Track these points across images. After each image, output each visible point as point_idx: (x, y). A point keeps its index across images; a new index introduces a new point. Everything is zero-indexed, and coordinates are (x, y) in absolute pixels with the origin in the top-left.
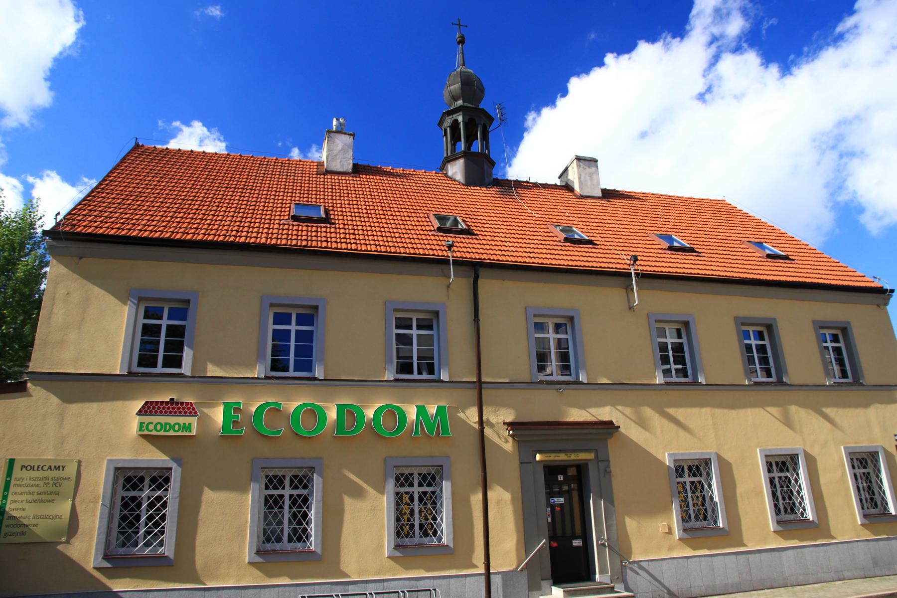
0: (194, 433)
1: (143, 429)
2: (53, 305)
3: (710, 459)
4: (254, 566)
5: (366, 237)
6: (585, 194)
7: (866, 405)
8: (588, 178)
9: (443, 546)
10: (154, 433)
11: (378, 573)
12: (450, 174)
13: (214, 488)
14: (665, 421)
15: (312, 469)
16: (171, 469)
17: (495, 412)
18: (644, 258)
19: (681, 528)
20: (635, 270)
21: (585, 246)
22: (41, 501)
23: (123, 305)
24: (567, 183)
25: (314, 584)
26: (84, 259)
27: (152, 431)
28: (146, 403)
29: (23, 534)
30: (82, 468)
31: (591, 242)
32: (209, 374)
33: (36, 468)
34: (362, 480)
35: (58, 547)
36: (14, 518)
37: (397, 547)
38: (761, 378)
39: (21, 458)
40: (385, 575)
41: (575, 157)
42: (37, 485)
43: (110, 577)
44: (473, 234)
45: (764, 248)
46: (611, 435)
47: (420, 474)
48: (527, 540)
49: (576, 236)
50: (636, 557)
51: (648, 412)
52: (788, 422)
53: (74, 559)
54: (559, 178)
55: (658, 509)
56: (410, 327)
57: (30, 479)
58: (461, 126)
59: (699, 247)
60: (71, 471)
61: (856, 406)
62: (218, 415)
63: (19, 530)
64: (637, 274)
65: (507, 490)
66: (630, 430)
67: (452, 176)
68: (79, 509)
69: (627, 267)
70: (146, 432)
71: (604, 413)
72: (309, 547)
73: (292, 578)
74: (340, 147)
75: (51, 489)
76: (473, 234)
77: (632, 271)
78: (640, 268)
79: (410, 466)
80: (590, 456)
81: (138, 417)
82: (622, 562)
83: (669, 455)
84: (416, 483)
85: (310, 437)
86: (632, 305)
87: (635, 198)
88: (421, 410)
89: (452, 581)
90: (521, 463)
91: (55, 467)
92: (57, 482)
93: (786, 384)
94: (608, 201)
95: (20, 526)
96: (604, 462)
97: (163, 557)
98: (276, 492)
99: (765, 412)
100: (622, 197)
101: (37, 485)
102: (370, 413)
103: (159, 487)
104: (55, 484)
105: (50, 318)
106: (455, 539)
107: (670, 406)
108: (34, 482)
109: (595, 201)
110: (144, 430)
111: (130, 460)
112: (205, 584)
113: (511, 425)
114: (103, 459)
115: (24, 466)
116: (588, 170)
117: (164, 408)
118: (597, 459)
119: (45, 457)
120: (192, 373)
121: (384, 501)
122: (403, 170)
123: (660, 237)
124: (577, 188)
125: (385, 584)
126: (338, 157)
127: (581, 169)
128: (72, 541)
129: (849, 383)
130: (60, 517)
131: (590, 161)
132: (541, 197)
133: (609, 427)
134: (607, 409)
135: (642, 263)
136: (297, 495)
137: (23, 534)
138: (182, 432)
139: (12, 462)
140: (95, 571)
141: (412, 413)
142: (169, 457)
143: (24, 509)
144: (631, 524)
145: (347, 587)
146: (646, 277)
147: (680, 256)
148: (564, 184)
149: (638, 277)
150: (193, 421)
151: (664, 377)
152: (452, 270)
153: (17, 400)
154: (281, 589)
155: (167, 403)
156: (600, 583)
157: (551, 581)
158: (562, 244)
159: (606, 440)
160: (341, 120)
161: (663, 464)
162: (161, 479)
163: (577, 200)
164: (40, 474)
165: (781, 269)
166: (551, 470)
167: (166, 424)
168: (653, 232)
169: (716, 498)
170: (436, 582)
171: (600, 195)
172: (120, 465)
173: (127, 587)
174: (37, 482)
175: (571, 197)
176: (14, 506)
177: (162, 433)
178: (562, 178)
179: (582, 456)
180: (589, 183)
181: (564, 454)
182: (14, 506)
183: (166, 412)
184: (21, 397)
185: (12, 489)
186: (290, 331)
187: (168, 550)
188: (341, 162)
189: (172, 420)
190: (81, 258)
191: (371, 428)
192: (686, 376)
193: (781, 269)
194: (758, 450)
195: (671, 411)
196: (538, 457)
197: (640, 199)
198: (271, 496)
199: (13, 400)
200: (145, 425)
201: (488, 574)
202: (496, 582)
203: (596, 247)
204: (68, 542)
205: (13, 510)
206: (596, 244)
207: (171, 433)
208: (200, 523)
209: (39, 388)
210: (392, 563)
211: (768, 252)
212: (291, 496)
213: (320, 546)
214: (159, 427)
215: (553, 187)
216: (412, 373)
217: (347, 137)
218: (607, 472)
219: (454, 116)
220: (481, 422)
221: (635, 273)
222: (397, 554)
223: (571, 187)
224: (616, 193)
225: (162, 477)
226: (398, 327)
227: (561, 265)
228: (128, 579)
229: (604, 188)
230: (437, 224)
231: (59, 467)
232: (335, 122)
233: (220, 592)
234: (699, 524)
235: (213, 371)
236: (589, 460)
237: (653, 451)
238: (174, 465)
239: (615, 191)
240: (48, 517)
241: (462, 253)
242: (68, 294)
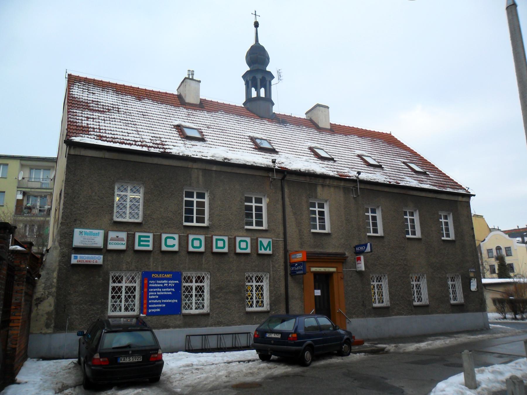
24: (311, 118)
54: (306, 114)
84: (194, 280)
148: (309, 118)
178: (309, 114)
186: (197, 202)
198: (198, 286)
212: (256, 286)
216: (252, 225)
229: (334, 123)
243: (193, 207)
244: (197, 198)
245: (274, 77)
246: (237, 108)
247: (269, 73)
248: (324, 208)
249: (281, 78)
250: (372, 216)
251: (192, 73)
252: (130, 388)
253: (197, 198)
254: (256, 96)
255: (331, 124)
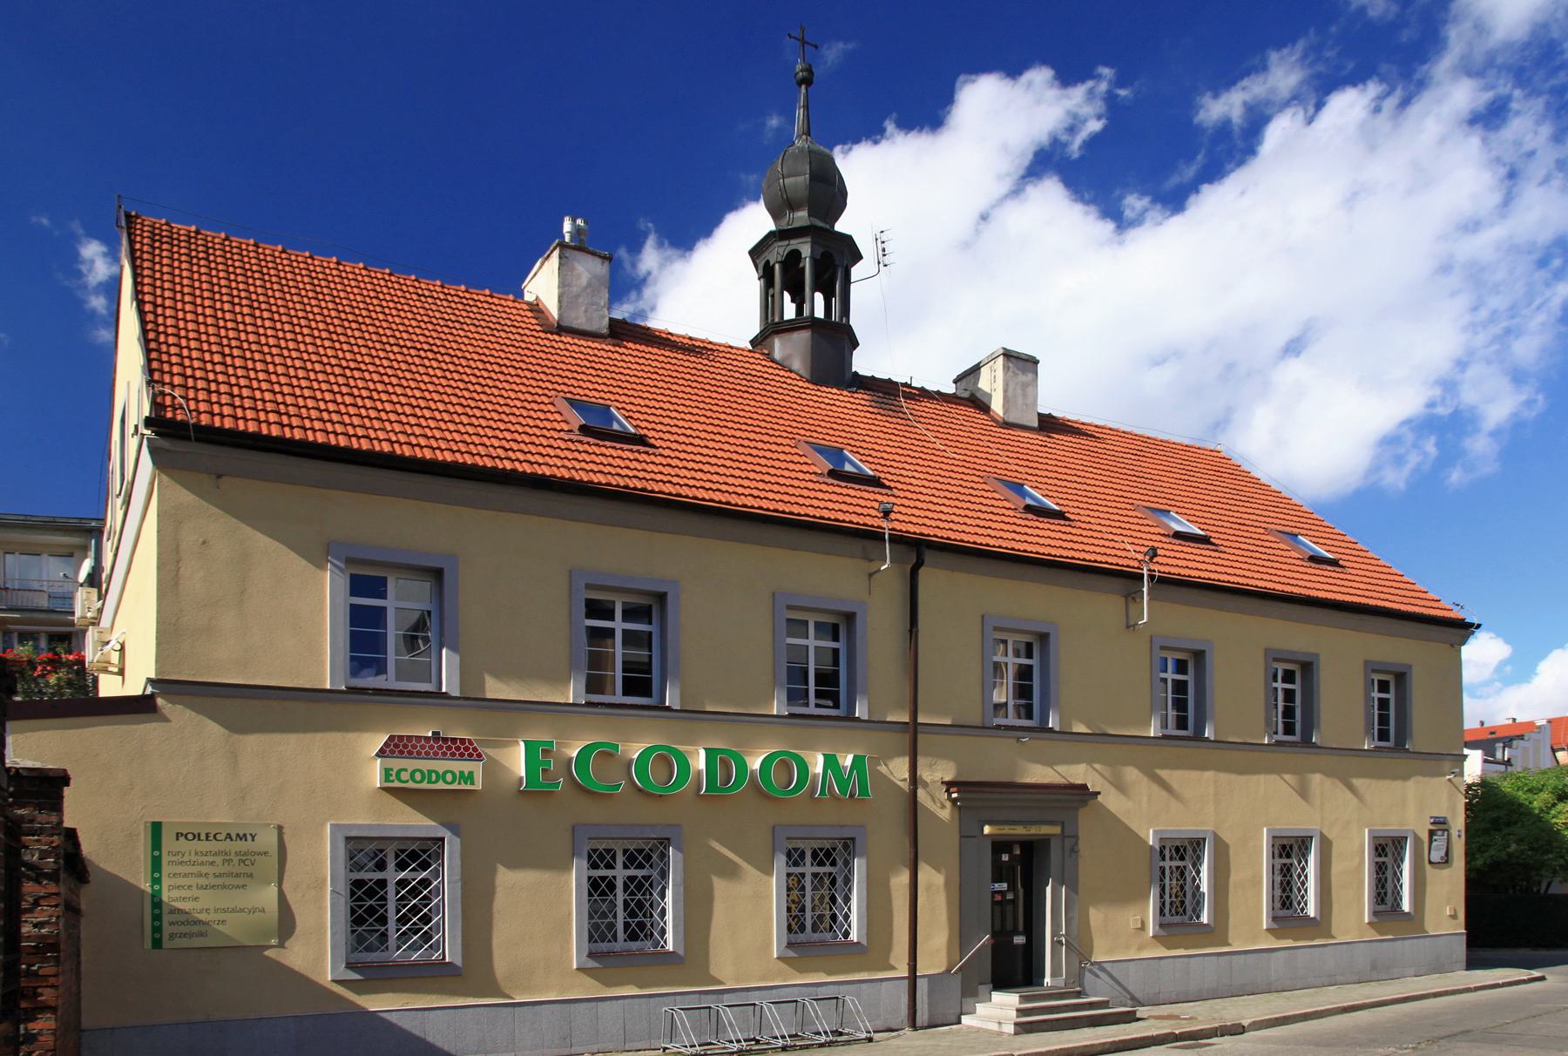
0: (478, 786)
1: (391, 778)
2: (178, 562)
3: (1204, 839)
4: (589, 975)
5: (259, 403)
6: (1011, 419)
7: (1405, 778)
8: (1019, 391)
9: (853, 944)
10: (411, 785)
11: (764, 978)
12: (777, 355)
13: (512, 865)
14: (1155, 788)
15: (665, 842)
16: (442, 840)
17: (931, 766)
18: (903, 510)
19: (1158, 922)
20: (1149, 570)
21: (863, 488)
22: (224, 887)
23: (318, 571)
24: (972, 395)
25: (650, 996)
26: (224, 479)
27: (407, 781)
28: (391, 738)
29: (201, 934)
30: (286, 838)
31: (641, 440)
32: (489, 695)
33: (203, 837)
34: (740, 857)
35: (267, 953)
36: (180, 911)
37: (790, 945)
38: (1281, 737)
39: (172, 818)
40: (773, 980)
41: (1002, 351)
42: (212, 863)
43: (359, 992)
44: (883, 486)
45: (1024, 494)
46: (1085, 803)
47: (625, 851)
48: (962, 937)
49: (616, 426)
50: (1098, 957)
51: (1132, 774)
52: (1303, 792)
53: (297, 969)
54: (955, 382)
55: (1130, 896)
56: (610, 615)
57: (196, 854)
58: (807, 265)
59: (890, 477)
60: (268, 840)
61: (1395, 778)
62: (516, 760)
63: (195, 929)
64: (1151, 577)
65: (938, 871)
66: (1111, 800)
67: (783, 360)
68: (292, 899)
69: (1136, 564)
70: (397, 784)
71: (1077, 773)
72: (662, 947)
73: (640, 987)
74: (584, 281)
75: (237, 869)
76: (883, 486)
77: (1145, 572)
78: (1156, 567)
79: (806, 839)
80: (1057, 830)
81: (379, 760)
82: (1080, 963)
83: (1154, 831)
85: (661, 796)
86: (1132, 623)
87: (1087, 435)
88: (830, 761)
89: (864, 986)
90: (961, 837)
91: (238, 835)
92: (246, 858)
93: (1315, 746)
94: (1049, 437)
95: (195, 923)
96: (1070, 839)
97: (442, 964)
98: (640, 873)
99: (1282, 782)
100: (1069, 432)
101: (212, 863)
102: (755, 763)
103: (424, 866)
104: (244, 861)
105: (177, 585)
106: (869, 935)
107: (1164, 767)
108: (205, 859)
109: (1027, 435)
110: (393, 781)
111: (370, 827)
112: (512, 998)
113: (949, 785)
114: (323, 824)
115: (182, 835)
116: (1022, 378)
117: (423, 747)
118: (1063, 836)
119: (217, 820)
120: (461, 693)
121: (772, 885)
122: (442, 287)
123: (820, 452)
124: (997, 406)
125: (774, 991)
126: (581, 300)
127: (1010, 373)
128: (287, 944)
129: (1389, 748)
130: (263, 911)
131: (1027, 360)
132: (648, 356)
133: (1081, 794)
134: (1082, 767)
135: (1165, 560)
136: (643, 877)
137: (201, 934)
138: (459, 783)
139: (157, 828)
140: (335, 985)
141: (817, 764)
142: (435, 821)
143: (196, 899)
144: (1096, 916)
145: (721, 996)
146: (1164, 583)
147: (853, 491)
149: (1152, 581)
150: (477, 768)
151: (788, 705)
152: (888, 551)
153: (142, 726)
154: (627, 1001)
155: (427, 739)
156: (1052, 987)
157: (991, 986)
158: (575, 438)
159: (1076, 809)
160: (579, 222)
161: (1145, 842)
162: (420, 854)
163: (999, 430)
164: (213, 846)
165: (1330, 581)
166: (999, 846)
167: (430, 772)
168: (1144, 503)
169: (1204, 888)
170: (842, 988)
171: (1035, 424)
172: (354, 833)
173: (392, 1005)
174: (211, 859)
175: (986, 423)
176: (176, 893)
177: (425, 785)
178: (963, 384)
179: (1045, 830)
180: (1020, 401)
181: (1021, 827)
182: (176, 893)
183: (462, 755)
184: (150, 721)
185: (166, 868)
187: (451, 951)
188: (586, 311)
189: (440, 765)
190: (219, 476)
191: (756, 788)
192: (836, 706)
193: (1330, 581)
194: (1265, 829)
195: (1164, 773)
196: (987, 829)
197: (1094, 437)
199: (135, 727)
200: (394, 773)
201: (913, 978)
202: (922, 986)
203: (651, 451)
204: (281, 945)
205: (176, 900)
206: (1069, 520)
207: (441, 785)
208: (496, 916)
209: (179, 707)
210: (782, 965)
211: (1029, 501)
213: (682, 945)
214: (418, 776)
215: (950, 399)
217: (598, 261)
218: (1074, 850)
219: (792, 242)
220: (914, 779)
221: (1149, 575)
222: (791, 954)
223: (984, 404)
224: (1053, 420)
225: (405, 851)
226: (589, 615)
227: (867, 525)
228: (391, 995)
229: (1046, 412)
230: (577, 420)
231: (245, 835)
232: (567, 226)
233: (537, 1007)
234: (1177, 919)
235: (496, 689)
236: (1054, 835)
237: (1134, 826)
238: (447, 835)
239: (889, 381)
240: (242, 910)
241: (535, 466)
242: (204, 543)
243: (838, 686)
244: (1380, 691)
245: (860, 257)
246: (734, 351)
247: (848, 241)
248: (383, 596)
249: (886, 260)
250: (1380, 699)
251: (62, 779)
252: (393, 991)
253: (397, 599)
254: (793, 317)
255: (1039, 414)
